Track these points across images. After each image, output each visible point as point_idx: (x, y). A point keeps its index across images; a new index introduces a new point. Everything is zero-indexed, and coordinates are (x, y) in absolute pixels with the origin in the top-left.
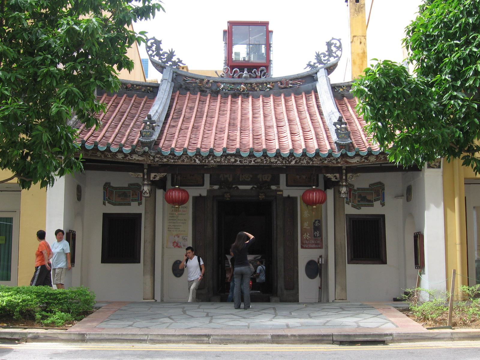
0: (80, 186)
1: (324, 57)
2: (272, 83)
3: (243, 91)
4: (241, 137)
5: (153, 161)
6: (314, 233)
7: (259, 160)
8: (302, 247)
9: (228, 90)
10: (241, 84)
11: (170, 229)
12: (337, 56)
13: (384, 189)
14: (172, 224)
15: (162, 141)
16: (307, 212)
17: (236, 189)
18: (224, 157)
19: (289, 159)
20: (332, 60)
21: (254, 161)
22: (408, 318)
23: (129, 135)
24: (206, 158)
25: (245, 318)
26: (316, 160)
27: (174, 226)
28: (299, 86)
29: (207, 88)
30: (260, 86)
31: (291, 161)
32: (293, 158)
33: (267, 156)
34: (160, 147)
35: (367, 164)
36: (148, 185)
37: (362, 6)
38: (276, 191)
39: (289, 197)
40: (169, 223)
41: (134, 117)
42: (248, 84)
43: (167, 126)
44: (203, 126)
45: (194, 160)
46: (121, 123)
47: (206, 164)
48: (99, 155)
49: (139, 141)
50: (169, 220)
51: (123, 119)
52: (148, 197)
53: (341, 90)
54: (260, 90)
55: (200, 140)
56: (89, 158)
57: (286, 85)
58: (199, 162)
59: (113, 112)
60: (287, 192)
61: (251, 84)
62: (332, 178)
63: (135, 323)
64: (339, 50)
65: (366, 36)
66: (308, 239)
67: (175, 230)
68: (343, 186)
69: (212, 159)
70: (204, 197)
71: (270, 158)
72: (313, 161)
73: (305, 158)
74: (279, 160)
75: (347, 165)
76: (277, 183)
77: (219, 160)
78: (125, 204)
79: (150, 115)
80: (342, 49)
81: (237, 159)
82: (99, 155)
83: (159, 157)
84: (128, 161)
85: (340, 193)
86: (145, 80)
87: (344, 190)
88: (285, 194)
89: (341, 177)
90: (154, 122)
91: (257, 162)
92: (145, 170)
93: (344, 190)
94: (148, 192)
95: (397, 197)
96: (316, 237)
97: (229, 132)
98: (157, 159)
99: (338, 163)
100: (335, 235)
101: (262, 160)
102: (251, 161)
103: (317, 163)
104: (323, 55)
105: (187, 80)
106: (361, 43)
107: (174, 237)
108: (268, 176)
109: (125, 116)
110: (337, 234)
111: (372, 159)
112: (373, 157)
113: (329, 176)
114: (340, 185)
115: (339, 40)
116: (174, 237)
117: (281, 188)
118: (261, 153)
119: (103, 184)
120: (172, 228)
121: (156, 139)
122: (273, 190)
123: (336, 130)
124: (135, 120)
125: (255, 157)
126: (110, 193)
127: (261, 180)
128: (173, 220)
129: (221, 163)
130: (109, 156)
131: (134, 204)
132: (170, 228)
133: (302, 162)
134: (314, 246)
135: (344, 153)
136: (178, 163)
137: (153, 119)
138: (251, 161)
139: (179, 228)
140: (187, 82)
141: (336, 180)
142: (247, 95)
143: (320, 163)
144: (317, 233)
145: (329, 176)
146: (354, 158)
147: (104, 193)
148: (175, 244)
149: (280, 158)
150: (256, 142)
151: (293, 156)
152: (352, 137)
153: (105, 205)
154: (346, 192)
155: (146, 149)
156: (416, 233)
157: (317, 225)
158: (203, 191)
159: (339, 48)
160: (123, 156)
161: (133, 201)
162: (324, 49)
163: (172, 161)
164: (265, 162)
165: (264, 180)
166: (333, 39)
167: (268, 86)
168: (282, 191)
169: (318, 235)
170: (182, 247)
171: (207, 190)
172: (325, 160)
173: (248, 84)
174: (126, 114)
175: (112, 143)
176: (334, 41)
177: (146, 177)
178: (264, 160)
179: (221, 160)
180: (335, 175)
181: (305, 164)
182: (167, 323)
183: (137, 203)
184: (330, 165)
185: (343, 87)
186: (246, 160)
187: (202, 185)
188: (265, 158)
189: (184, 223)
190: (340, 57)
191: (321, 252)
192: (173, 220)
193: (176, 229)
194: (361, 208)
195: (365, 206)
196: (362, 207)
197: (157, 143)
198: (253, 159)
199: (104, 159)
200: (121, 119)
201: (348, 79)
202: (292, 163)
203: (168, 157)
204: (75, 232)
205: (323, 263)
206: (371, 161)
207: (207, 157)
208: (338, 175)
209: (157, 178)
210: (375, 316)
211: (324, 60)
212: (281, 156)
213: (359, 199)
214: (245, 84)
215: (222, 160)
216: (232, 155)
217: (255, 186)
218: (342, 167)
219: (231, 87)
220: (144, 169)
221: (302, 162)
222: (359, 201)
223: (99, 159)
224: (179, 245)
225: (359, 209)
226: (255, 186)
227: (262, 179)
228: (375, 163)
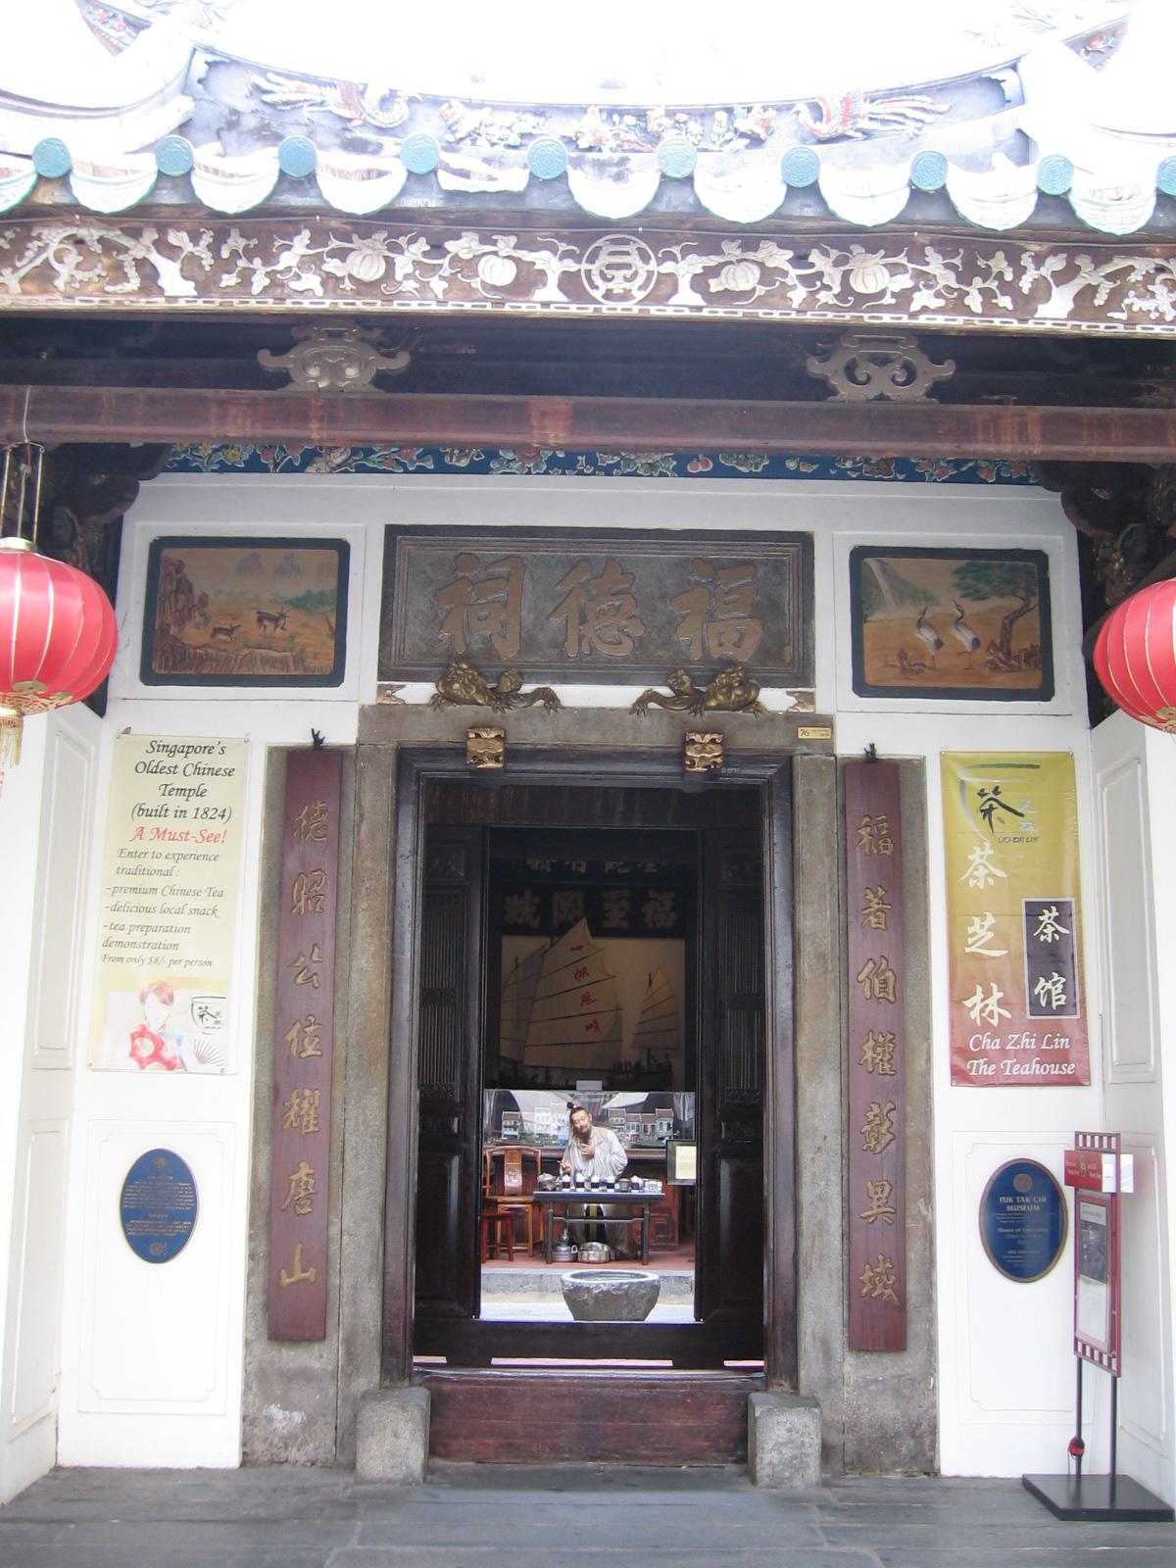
6: (1033, 983)
7: (744, 278)
8: (959, 1076)
9: (509, 147)
14: (130, 919)
16: (989, 851)
17: (540, 703)
21: (699, 283)
27: (146, 929)
29: (381, 130)
31: (1042, 292)
38: (792, 719)
40: (116, 908)
42: (622, 113)
45: (141, 264)
47: (253, 304)
50: (116, 890)
57: (844, 122)
58: (188, 288)
60: (865, 726)
66: (995, 1022)
67: (148, 953)
69: (306, 263)
70: (339, 753)
73: (1161, 269)
74: (925, 279)
76: (800, 673)
81: (543, 260)
86: (606, 1070)
88: (849, 744)
91: (729, 296)
96: (1048, 1010)
102: (670, 282)
107: (143, 1000)
108: (742, 635)
116: (143, 1000)
117: (822, 707)
120: (133, 945)
122: (773, 718)
128: (134, 890)
129: (388, 299)
133: (1139, 304)
134: (1034, 1068)
139: (176, 946)
142: (614, 170)
144: (1052, 987)
148: (147, 1048)
157: (1048, 934)
158: (334, 716)
164: (799, 295)
165: (716, 653)
168: (827, 722)
170: (191, 1062)
171: (364, 713)
173: (622, 113)
178: (793, 272)
179: (390, 264)
186: (619, 274)
189: (204, 913)
192: (134, 890)
193: (156, 946)
198: (688, 267)
202: (1043, 310)
217: (664, 691)
221: (1139, 304)
224: (167, 1054)
227: (704, 650)
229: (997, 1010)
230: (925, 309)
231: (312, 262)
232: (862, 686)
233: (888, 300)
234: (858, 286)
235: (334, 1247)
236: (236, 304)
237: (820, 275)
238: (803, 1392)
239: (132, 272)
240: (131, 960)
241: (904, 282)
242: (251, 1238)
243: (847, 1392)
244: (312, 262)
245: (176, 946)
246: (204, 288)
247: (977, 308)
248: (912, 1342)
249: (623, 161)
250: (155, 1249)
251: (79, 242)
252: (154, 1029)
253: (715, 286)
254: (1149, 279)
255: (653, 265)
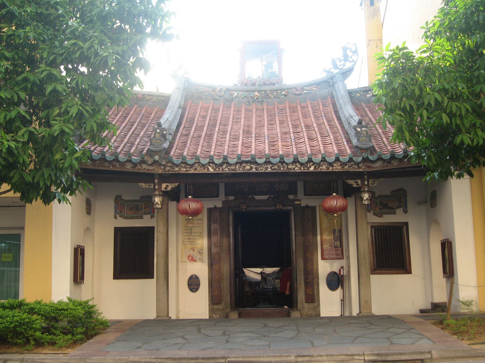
0: (89, 199)
1: (340, 61)
2: (287, 89)
3: (257, 99)
4: (256, 144)
5: (163, 171)
6: (334, 243)
7: (276, 167)
8: (323, 258)
10: (254, 91)
11: (185, 243)
12: (353, 61)
13: (406, 196)
15: (173, 150)
17: (252, 199)
18: (239, 165)
19: (307, 165)
20: (348, 65)
21: (271, 168)
22: (443, 332)
23: (138, 144)
24: (220, 166)
25: (265, 336)
26: (336, 165)
28: (315, 92)
30: (275, 93)
31: (310, 167)
32: (312, 163)
33: (284, 162)
34: (171, 155)
35: (390, 168)
36: (159, 195)
37: (377, 9)
39: (307, 206)
41: (144, 127)
42: (262, 91)
43: (179, 135)
44: (216, 134)
45: (207, 168)
46: (130, 133)
47: (220, 172)
48: (107, 165)
49: (149, 150)
51: (133, 128)
52: (160, 208)
53: (358, 95)
54: (275, 97)
55: (213, 147)
56: (97, 168)
59: (123, 122)
60: (305, 201)
61: (265, 91)
62: (353, 184)
63: (144, 345)
64: (354, 54)
65: (382, 40)
68: (364, 192)
71: (287, 164)
72: (333, 167)
73: (324, 163)
74: (297, 166)
75: (369, 170)
76: (295, 193)
77: (233, 167)
78: (137, 217)
79: (160, 123)
80: (357, 54)
81: (253, 166)
82: (107, 165)
83: (171, 166)
84: (137, 171)
85: (362, 199)
87: (366, 196)
88: (303, 204)
89: (363, 183)
90: (164, 129)
91: (274, 169)
92: (156, 180)
93: (366, 196)
94: (159, 203)
95: (420, 203)
97: (244, 139)
98: (168, 168)
99: (359, 168)
100: (357, 244)
101: (279, 166)
102: (267, 168)
103: (337, 168)
104: (338, 61)
105: (199, 88)
106: (377, 47)
107: (190, 250)
109: (135, 126)
110: (359, 243)
111: (395, 164)
112: (396, 161)
113: (351, 182)
114: (362, 192)
115: (355, 44)
116: (190, 250)
117: (299, 198)
118: (278, 160)
119: (114, 198)
121: (167, 147)
123: (356, 134)
124: (145, 129)
125: (272, 163)
126: (122, 207)
127: (277, 189)
129: (236, 171)
130: (118, 166)
131: (147, 217)
132: (185, 242)
135: (365, 157)
136: (190, 172)
137: (163, 126)
138: (267, 168)
140: (200, 90)
141: (357, 186)
142: (261, 103)
143: (340, 168)
145: (351, 182)
146: (377, 162)
147: (115, 206)
148: (191, 258)
149: (298, 164)
150: (272, 148)
151: (312, 161)
152: (373, 141)
153: (116, 219)
154: (369, 199)
155: (157, 158)
156: (443, 240)
158: (218, 203)
159: (355, 52)
160: (132, 166)
161: (145, 214)
162: (340, 54)
163: (184, 170)
164: (282, 169)
166: (348, 43)
167: (283, 93)
169: (339, 245)
171: (223, 202)
172: (346, 165)
174: (136, 124)
175: (120, 153)
176: (349, 46)
177: (157, 187)
179: (236, 167)
180: (356, 180)
181: (324, 169)
182: (179, 343)
183: (149, 216)
184: (351, 170)
185: (360, 92)
187: (217, 196)
188: (282, 165)
190: (356, 62)
191: (343, 262)
194: (382, 216)
195: (387, 213)
196: (384, 215)
197: (168, 151)
198: (269, 166)
199: (112, 169)
200: (130, 129)
201: (365, 83)
202: (310, 169)
203: (180, 166)
204: (84, 247)
205: (345, 274)
206: (394, 165)
207: (221, 165)
208: (359, 182)
209: (169, 188)
210: (407, 330)
211: (340, 65)
212: (299, 162)
213: (381, 207)
214: (259, 91)
215: (237, 167)
216: (247, 162)
217: (272, 196)
218: (363, 172)
219: (245, 95)
220: (155, 179)
222: (380, 209)
223: (107, 169)
224: (194, 259)
225: (380, 217)
226: (272, 196)
228: (398, 167)
229: (328, 247)
230: (297, 170)
231: (226, 167)
232: (305, 194)
233: (292, 169)
234: (289, 167)
235: (222, 289)
236: (218, 172)
237: (285, 166)
238: (298, 310)
239: (206, 169)
240: (187, 244)
241: (294, 167)
242: (209, 288)
243: (306, 309)
244: (226, 167)
245: (194, 242)
246: (214, 170)
247: (303, 169)
248: (316, 302)
249: (262, 101)
250: (194, 290)
251: (200, 165)
252: (192, 255)
253: (273, 168)
254: (323, 164)
255: (265, 166)
